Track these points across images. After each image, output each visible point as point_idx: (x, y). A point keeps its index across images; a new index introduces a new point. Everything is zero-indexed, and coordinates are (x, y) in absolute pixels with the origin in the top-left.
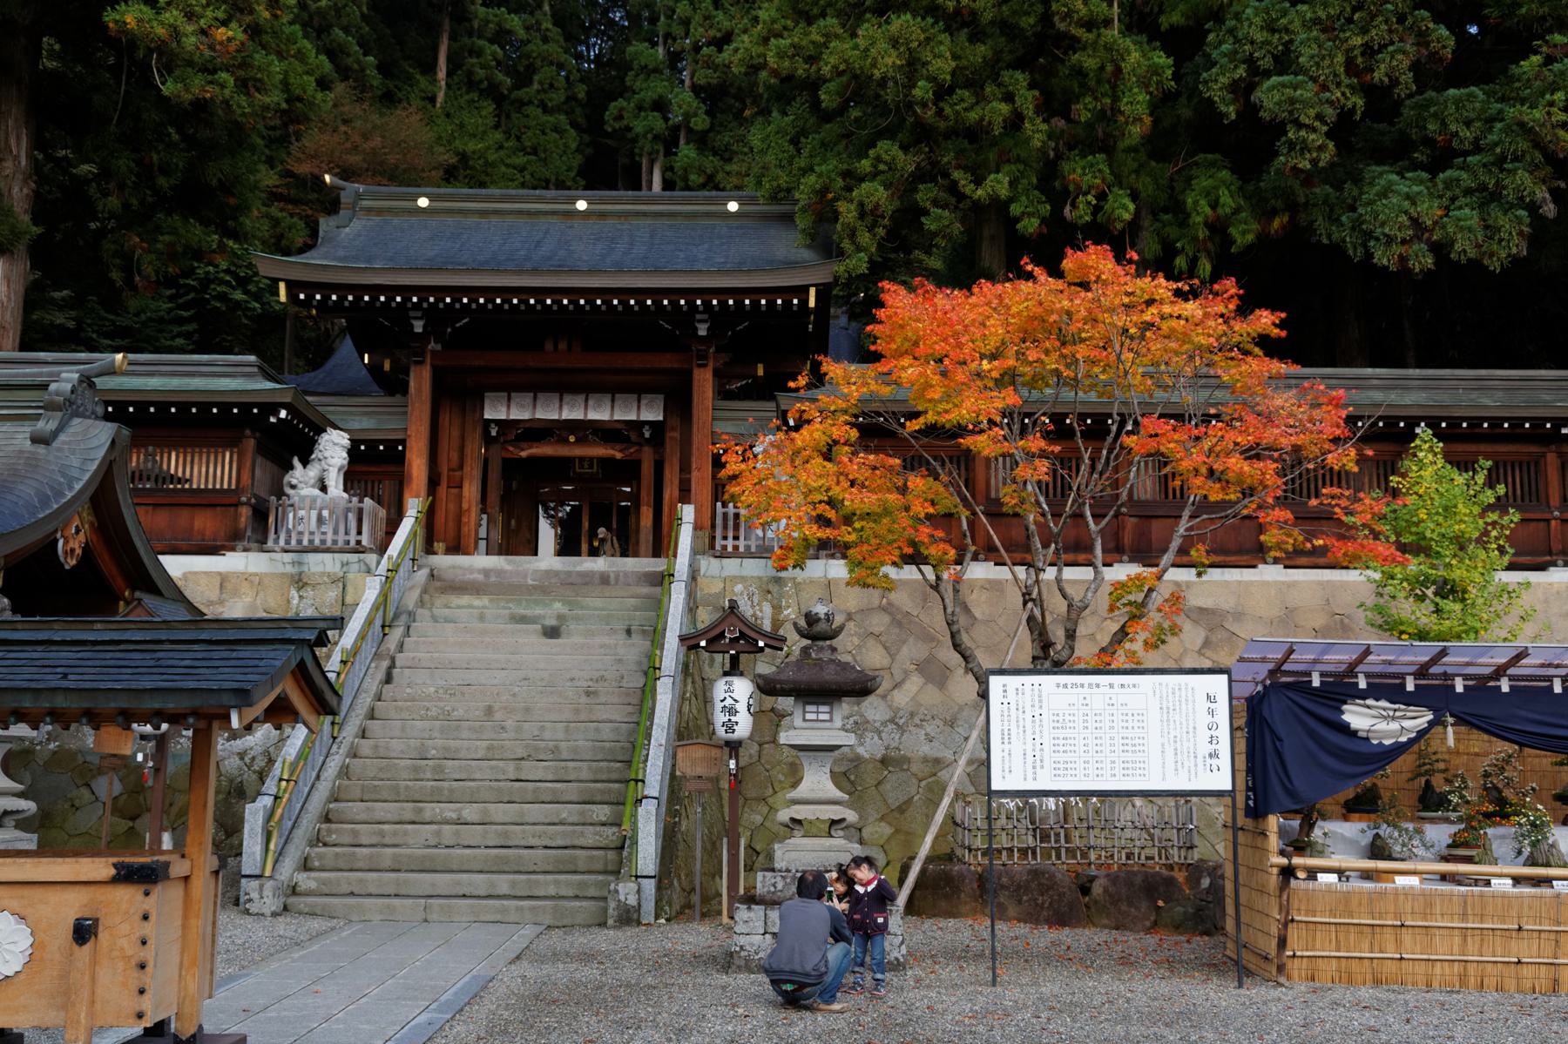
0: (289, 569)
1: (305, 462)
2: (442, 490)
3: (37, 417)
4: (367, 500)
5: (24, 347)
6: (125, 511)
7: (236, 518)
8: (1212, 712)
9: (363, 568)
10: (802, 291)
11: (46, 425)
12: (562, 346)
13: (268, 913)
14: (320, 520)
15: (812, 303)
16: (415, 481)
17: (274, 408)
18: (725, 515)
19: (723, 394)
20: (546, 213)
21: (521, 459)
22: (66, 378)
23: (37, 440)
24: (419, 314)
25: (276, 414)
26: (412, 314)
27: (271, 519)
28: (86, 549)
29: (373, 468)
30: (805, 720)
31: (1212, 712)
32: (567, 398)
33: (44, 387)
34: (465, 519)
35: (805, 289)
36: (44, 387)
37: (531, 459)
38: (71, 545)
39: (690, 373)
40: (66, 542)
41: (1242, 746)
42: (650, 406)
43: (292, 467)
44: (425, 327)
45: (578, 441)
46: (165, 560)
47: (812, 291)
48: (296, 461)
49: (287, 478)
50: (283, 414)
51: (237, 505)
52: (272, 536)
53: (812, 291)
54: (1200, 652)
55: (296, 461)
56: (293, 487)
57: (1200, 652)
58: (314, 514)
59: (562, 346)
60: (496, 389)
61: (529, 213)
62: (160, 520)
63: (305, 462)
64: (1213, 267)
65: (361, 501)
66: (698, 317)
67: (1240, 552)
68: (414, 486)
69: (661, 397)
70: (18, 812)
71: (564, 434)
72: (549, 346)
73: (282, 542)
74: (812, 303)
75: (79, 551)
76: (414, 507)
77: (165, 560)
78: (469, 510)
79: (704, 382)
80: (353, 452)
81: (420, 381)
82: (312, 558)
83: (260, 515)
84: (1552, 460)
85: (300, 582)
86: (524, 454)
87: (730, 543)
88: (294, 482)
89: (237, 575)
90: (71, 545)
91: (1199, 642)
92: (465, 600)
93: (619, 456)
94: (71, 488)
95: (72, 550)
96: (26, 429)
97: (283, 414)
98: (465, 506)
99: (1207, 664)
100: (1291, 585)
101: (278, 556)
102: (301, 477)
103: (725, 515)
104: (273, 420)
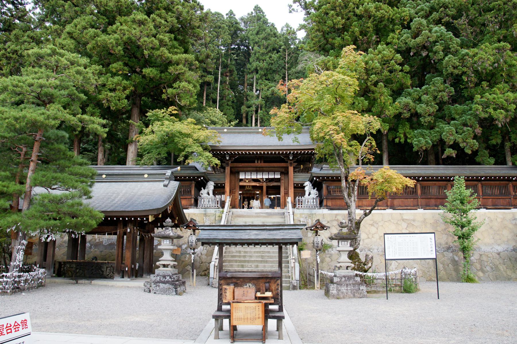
0: (203, 212)
1: (204, 189)
3: (164, 181)
5: (105, 164)
7: (191, 201)
8: (431, 242)
11: (166, 182)
12: (259, 162)
14: (209, 201)
19: (295, 172)
22: (169, 172)
23: (165, 186)
29: (219, 189)
31: (431, 242)
32: (258, 173)
33: (165, 174)
36: (165, 174)
39: (288, 167)
41: (83, 281)
42: (277, 174)
46: (184, 210)
48: (202, 188)
49: (201, 192)
50: (202, 178)
54: (406, 229)
55: (202, 188)
57: (406, 229)
59: (259, 162)
60: (242, 171)
63: (204, 189)
64: (452, 145)
67: (414, 206)
72: (256, 162)
77: (184, 210)
79: (291, 169)
81: (228, 170)
82: (208, 210)
84: (480, 185)
85: (205, 215)
87: (300, 206)
89: (192, 214)
91: (406, 226)
93: (258, 185)
96: (162, 184)
97: (202, 178)
99: (408, 232)
100: (425, 214)
101: (201, 209)
102: (204, 192)
103: (299, 200)
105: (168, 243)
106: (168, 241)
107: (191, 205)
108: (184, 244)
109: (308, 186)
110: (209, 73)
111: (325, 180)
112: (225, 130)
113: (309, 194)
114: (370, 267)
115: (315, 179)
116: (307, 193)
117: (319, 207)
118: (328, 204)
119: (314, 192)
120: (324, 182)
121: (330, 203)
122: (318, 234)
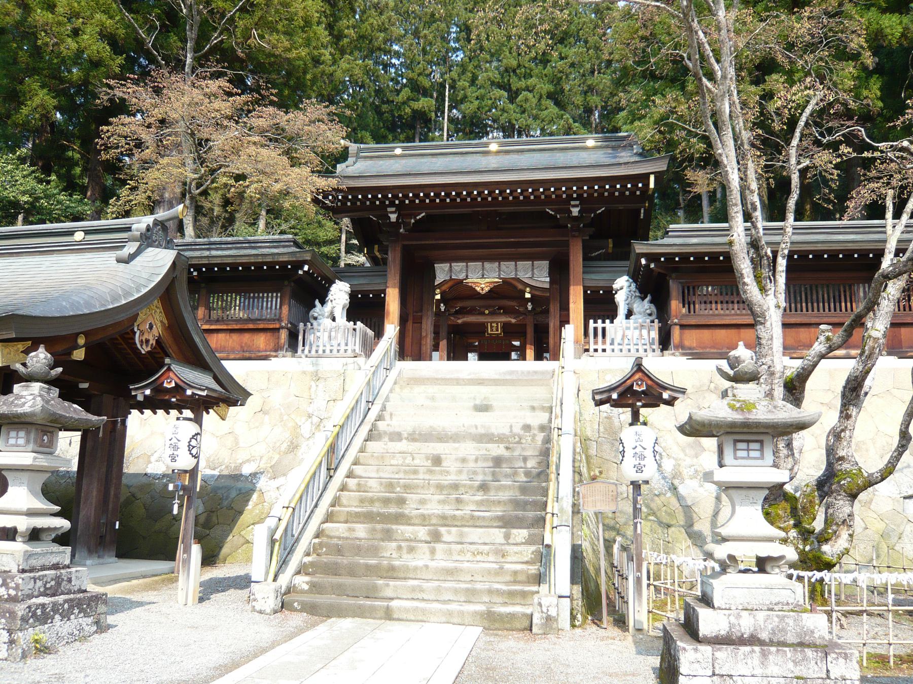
2: (410, 325)
4: (359, 323)
6: (186, 315)
9: (357, 367)
10: (645, 177)
13: (268, 611)
15: (652, 185)
16: (391, 315)
17: (300, 264)
18: (596, 329)
20: (473, 153)
21: (458, 325)
24: (393, 209)
25: (302, 268)
26: (389, 209)
27: (300, 338)
28: (158, 342)
30: (736, 458)
34: (423, 342)
35: (647, 176)
37: (465, 324)
38: (146, 336)
40: (142, 333)
43: (314, 306)
44: (398, 218)
45: (491, 314)
47: (652, 178)
49: (311, 313)
51: (277, 330)
52: (300, 348)
53: (652, 178)
56: (315, 319)
58: (326, 334)
61: (462, 153)
62: (233, 340)
63: (323, 303)
65: (355, 324)
66: (573, 203)
68: (391, 317)
69: (545, 264)
70: (55, 529)
71: (482, 310)
73: (306, 351)
74: (652, 185)
75: (152, 342)
76: (391, 329)
78: (426, 336)
80: (353, 295)
83: (293, 337)
86: (460, 321)
88: (316, 315)
90: (146, 336)
92: (422, 388)
93: (513, 321)
94: (138, 291)
95: (147, 341)
97: (306, 268)
98: (424, 334)
103: (596, 329)
104: (300, 272)
105: (21, 441)
106: (22, 434)
107: (277, 348)
108: (248, 461)
109: (625, 290)
110: (426, 93)
111: (676, 270)
112: (398, 151)
113: (629, 314)
114: (847, 551)
115: (643, 261)
116: (622, 311)
117: (658, 352)
118: (687, 343)
119: (644, 307)
120: (674, 275)
121: (692, 338)
122: (641, 419)
